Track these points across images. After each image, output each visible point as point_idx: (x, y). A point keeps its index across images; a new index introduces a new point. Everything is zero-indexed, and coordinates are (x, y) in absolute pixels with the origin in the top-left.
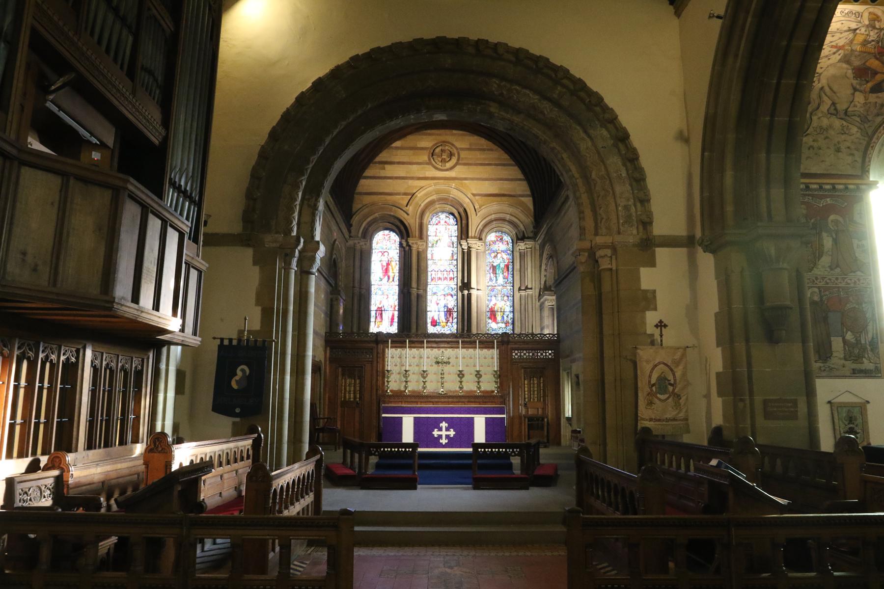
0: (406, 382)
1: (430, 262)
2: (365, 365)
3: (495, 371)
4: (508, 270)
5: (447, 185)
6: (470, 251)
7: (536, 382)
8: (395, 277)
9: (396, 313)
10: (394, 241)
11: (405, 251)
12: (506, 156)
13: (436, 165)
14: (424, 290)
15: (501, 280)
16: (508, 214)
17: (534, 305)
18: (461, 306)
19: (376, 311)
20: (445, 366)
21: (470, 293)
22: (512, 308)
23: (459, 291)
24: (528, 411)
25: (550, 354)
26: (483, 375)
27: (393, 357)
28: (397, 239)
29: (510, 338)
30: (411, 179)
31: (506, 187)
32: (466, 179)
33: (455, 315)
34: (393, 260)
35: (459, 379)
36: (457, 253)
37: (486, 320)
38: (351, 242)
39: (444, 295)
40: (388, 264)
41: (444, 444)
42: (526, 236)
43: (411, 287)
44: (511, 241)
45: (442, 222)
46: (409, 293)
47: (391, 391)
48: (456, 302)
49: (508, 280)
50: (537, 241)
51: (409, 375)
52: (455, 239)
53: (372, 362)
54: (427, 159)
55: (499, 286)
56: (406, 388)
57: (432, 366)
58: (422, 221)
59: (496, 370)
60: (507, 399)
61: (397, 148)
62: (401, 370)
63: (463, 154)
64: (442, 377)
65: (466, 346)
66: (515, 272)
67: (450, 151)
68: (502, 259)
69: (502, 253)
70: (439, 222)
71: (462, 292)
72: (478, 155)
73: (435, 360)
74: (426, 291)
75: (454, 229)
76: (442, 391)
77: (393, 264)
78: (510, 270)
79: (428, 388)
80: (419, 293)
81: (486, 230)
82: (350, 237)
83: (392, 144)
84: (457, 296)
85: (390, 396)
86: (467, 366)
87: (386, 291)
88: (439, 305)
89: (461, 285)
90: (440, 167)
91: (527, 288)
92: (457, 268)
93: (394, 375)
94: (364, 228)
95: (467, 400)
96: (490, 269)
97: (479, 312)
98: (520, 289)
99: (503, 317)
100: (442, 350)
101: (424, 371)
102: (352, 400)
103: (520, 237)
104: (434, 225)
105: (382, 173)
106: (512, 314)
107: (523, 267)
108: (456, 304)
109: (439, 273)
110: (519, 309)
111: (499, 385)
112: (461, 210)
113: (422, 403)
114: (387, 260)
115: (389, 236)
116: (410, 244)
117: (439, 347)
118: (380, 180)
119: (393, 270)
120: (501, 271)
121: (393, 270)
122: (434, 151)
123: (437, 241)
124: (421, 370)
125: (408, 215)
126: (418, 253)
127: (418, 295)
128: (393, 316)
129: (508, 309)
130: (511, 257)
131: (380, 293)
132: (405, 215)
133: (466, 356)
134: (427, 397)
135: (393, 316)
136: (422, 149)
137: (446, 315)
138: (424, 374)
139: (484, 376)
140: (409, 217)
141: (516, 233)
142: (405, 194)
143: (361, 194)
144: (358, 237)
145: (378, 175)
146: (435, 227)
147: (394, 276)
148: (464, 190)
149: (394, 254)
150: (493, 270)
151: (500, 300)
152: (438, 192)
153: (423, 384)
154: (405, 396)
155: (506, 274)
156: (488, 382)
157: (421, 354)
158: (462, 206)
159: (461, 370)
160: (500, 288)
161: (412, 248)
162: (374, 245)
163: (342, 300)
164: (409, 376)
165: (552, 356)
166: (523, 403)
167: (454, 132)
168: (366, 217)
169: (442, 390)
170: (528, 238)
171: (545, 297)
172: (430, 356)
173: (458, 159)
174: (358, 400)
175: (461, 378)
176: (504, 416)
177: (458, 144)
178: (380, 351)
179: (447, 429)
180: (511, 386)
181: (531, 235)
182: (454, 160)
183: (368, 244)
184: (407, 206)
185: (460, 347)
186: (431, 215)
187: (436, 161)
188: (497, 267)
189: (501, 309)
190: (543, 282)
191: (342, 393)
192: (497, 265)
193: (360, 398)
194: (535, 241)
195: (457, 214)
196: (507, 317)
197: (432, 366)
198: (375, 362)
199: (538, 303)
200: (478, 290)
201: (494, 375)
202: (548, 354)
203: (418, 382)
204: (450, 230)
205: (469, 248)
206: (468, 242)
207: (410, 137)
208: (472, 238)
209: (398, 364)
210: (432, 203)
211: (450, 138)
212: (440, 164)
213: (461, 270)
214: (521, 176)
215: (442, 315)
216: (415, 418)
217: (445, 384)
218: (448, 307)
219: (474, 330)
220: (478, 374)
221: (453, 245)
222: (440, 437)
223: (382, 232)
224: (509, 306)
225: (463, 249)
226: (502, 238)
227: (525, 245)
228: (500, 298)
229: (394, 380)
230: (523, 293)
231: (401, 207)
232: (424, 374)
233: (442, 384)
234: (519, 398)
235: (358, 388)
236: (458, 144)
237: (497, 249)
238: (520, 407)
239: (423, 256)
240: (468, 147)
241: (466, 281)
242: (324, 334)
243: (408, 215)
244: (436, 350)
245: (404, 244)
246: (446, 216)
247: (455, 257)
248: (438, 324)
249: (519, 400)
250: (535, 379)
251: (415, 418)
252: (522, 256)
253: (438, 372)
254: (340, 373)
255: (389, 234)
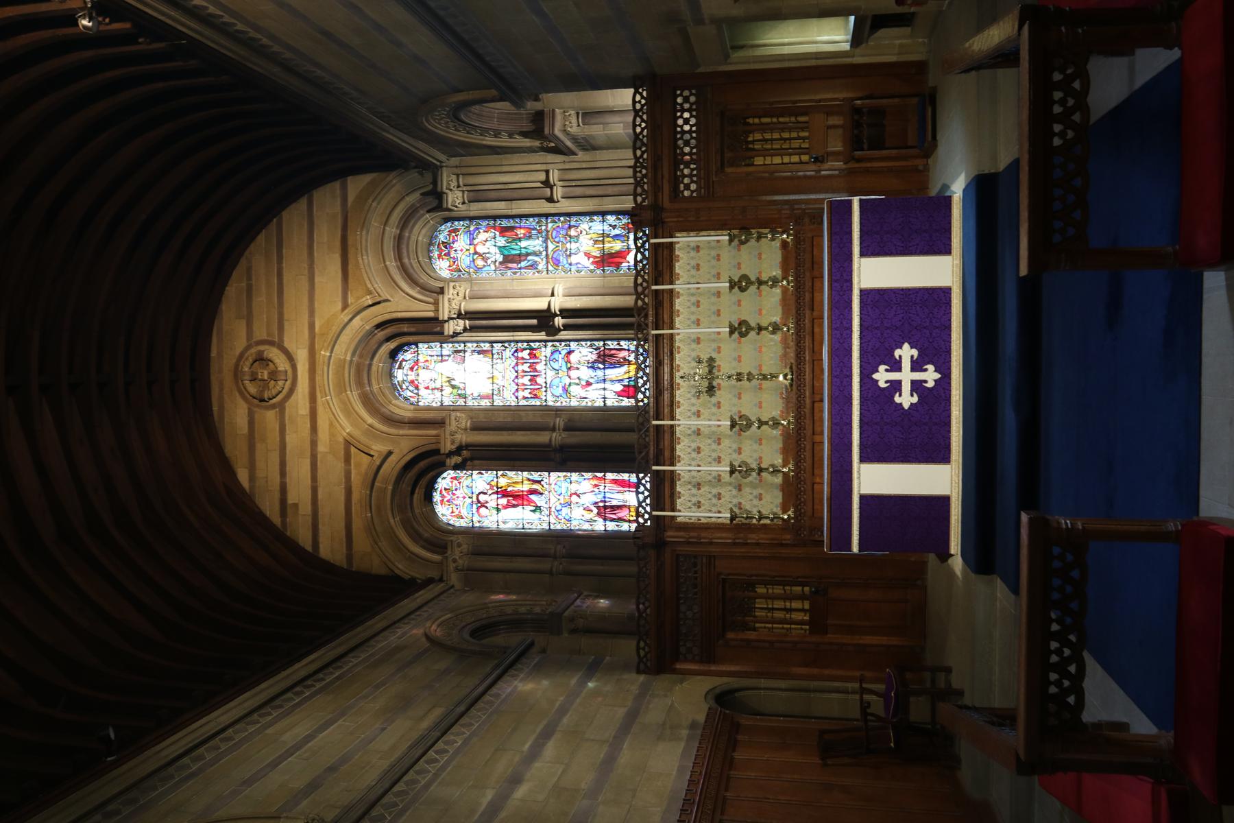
0: (761, 470)
1: (498, 402)
2: (720, 574)
3: (731, 241)
4: (512, 228)
5: (326, 368)
6: (467, 313)
7: (758, 136)
8: (531, 477)
9: (610, 476)
10: (455, 482)
11: (472, 459)
12: (261, 238)
13: (285, 392)
14: (557, 416)
15: (535, 244)
16: (384, 229)
17: (584, 166)
18: (591, 332)
19: (605, 520)
20: (719, 371)
21: (560, 311)
22: (595, 218)
23: (557, 337)
24: (834, 153)
25: (686, 99)
26: (743, 272)
27: (699, 502)
28: (448, 476)
29: (646, 203)
30: (316, 446)
31: (326, 234)
32: (312, 326)
33: (612, 345)
34: (494, 483)
35: (752, 334)
36: (477, 342)
37: (623, 275)
38: (454, 579)
39: (569, 369)
40: (505, 494)
41: (938, 376)
42: (431, 187)
43: (549, 445)
44: (449, 224)
45: (412, 376)
46: (562, 448)
47: (785, 511)
48: (583, 343)
49: (535, 229)
50: (441, 162)
51: (744, 463)
52: (448, 348)
53: (711, 558)
54: (274, 411)
55: (547, 247)
56: (776, 471)
57: (719, 403)
58: (406, 420)
59: (727, 238)
60: (803, 206)
61: (252, 478)
62: (730, 484)
63: (260, 333)
64: (749, 379)
65: (666, 317)
66: (514, 212)
67: (255, 361)
68: (489, 243)
69: (475, 242)
70: (412, 382)
71: (560, 330)
72: (260, 300)
73: (705, 397)
74: (558, 411)
75: (426, 351)
76: (785, 376)
77: (503, 482)
78: (511, 223)
79: (776, 413)
80: (562, 426)
81: (423, 278)
82: (441, 580)
83: (243, 489)
84: (570, 341)
85: (799, 514)
86: (718, 313)
87: (561, 497)
88: (591, 380)
89: (544, 333)
90: (288, 383)
91: (546, 183)
92: (509, 342)
93: (744, 503)
94: (423, 547)
95: (808, 312)
96: (510, 269)
97: (602, 291)
98: (550, 200)
99: (616, 237)
100: (678, 380)
101: (733, 426)
102: (807, 606)
103: (435, 203)
104: (418, 394)
105: (306, 509)
106: (609, 217)
107: (503, 194)
108: (589, 343)
109: (520, 381)
110: (596, 201)
111: (767, 231)
112: (381, 335)
113: (817, 429)
114: (495, 496)
115: (444, 492)
116: (453, 447)
117: (672, 386)
118: (320, 513)
119: (516, 483)
120: (513, 245)
121: (516, 483)
122: (254, 398)
123: (453, 387)
124: (729, 432)
125: (390, 453)
126: (476, 428)
127: (566, 429)
128: (615, 482)
129: (597, 226)
130: (485, 223)
131: (565, 511)
132: (393, 458)
133: (693, 318)
134: (799, 417)
135: (615, 482)
136: (251, 423)
137: (613, 366)
138: (740, 424)
139: (744, 270)
140: (396, 451)
141: (428, 211)
142: (347, 459)
143: (349, 557)
144: (441, 563)
145: (310, 519)
146: (423, 392)
147: (529, 480)
148: (335, 329)
149: (481, 481)
150: (512, 262)
151: (578, 244)
152: (341, 388)
153: (764, 427)
154: (797, 476)
155: (521, 232)
156: (760, 258)
157: (689, 432)
158: (370, 334)
159: (728, 329)
160: (551, 246)
161: (464, 444)
162: (462, 523)
163: (578, 602)
164: (746, 464)
165: (691, 94)
166: (813, 167)
167: (214, 353)
168: (399, 547)
169: (781, 378)
170: (435, 183)
171: (557, 132)
172: (694, 409)
173: (272, 343)
174: (807, 589)
175: (749, 328)
176: (856, 201)
177: (240, 344)
178: (680, 536)
179: (896, 366)
180: (769, 198)
181: (428, 176)
182: (273, 353)
183: (460, 539)
184: (372, 456)
185: (671, 331)
186: (394, 402)
187: (274, 392)
188: (506, 253)
189: (596, 242)
190: (527, 143)
191: (790, 628)
192: (502, 253)
193: (803, 585)
194: (442, 167)
195: (392, 345)
196: (614, 227)
197: (719, 405)
198: (712, 549)
199: (579, 156)
200: (553, 295)
201: (742, 243)
202: (686, 115)
203: (760, 440)
204: (429, 358)
205: (460, 316)
206: (446, 318)
207: (229, 450)
208: (437, 310)
209: (715, 491)
210: (369, 402)
211: (229, 362)
212: (281, 383)
213: (511, 334)
214: (303, 203)
215: (612, 373)
216: (863, 459)
217: (765, 370)
218: (595, 361)
219: (628, 301)
220: (740, 284)
221: (460, 351)
222: (917, 386)
223: (435, 506)
224: (590, 224)
225: (465, 330)
226: (443, 243)
227: (451, 190)
228: (574, 246)
229: (756, 502)
230: (558, 192)
231: (375, 468)
232: (740, 424)
233: (765, 377)
234: (799, 177)
235: (778, 590)
236: (240, 344)
237: (467, 253)
238: (823, 173)
239: (482, 418)
240: (243, 322)
241: (534, 322)
242: (642, 678)
243: (390, 453)
244: (678, 393)
245: (457, 459)
246: (400, 367)
247: (487, 346)
248: (632, 383)
249: (805, 177)
250: (750, 139)
251: (863, 459)
252: (477, 196)
253: (734, 387)
254: (741, 636)
255: (441, 493)
